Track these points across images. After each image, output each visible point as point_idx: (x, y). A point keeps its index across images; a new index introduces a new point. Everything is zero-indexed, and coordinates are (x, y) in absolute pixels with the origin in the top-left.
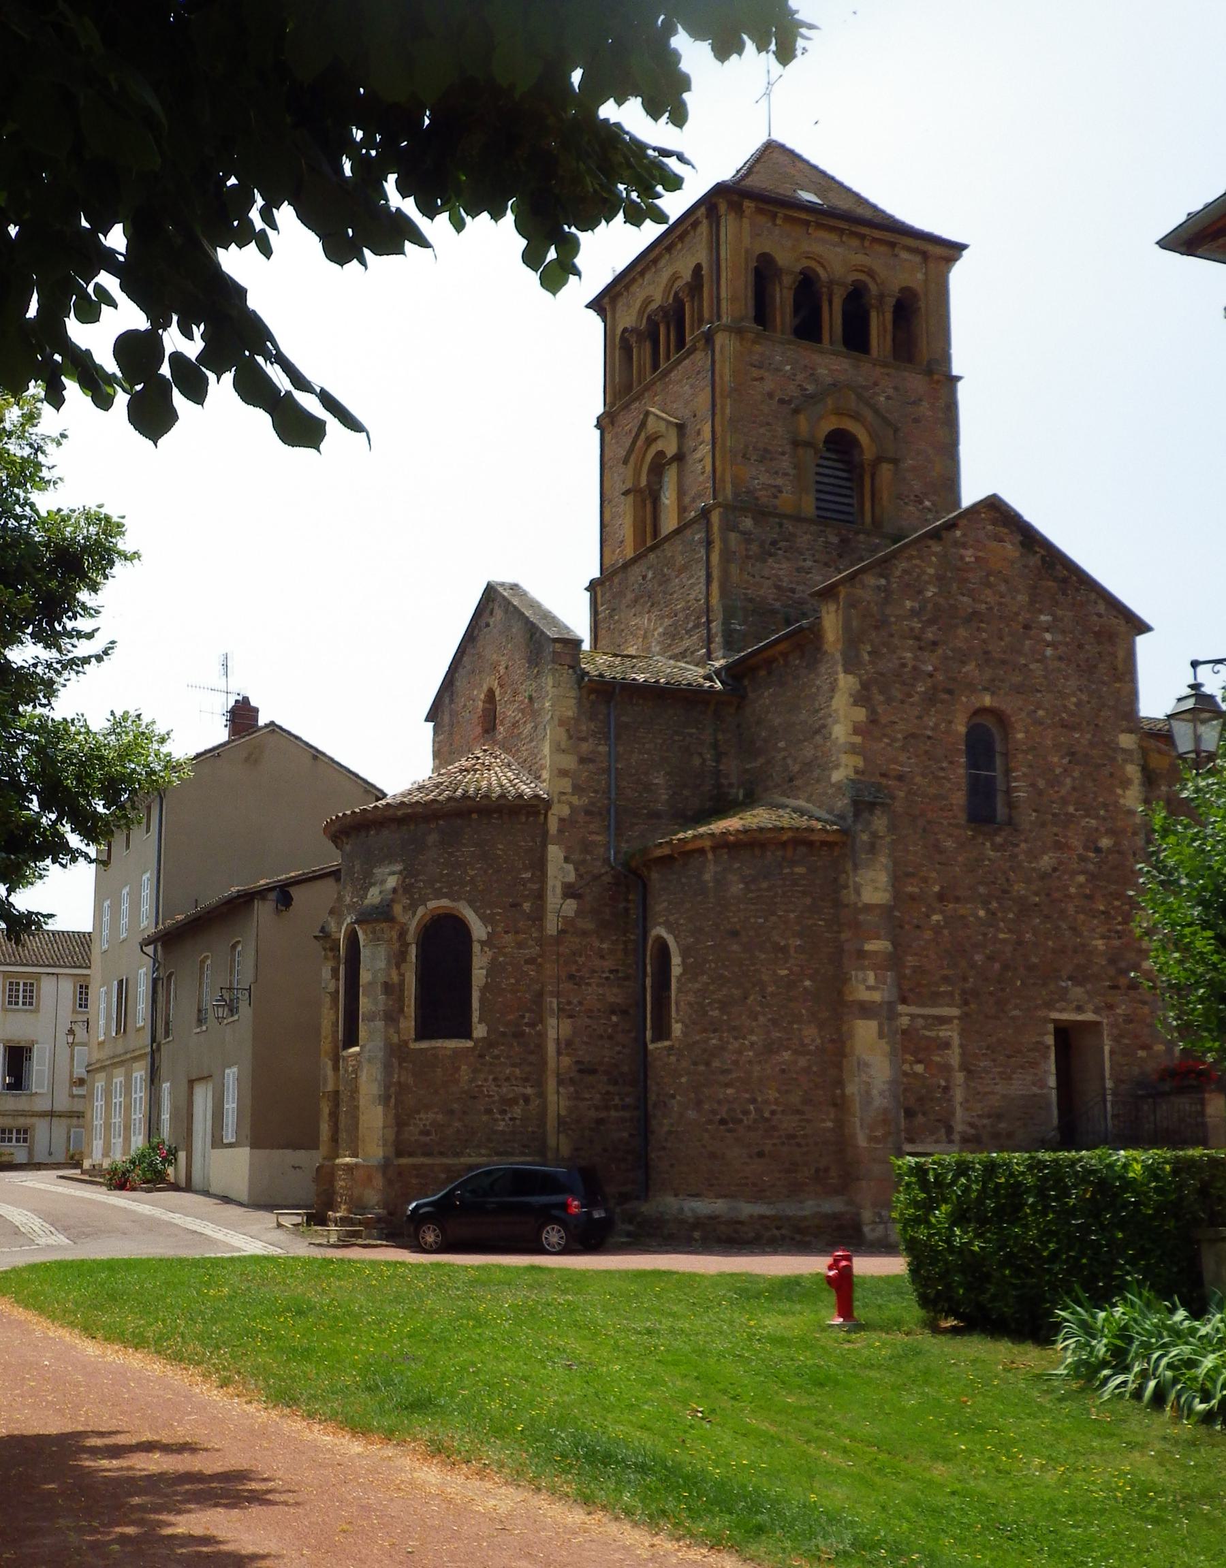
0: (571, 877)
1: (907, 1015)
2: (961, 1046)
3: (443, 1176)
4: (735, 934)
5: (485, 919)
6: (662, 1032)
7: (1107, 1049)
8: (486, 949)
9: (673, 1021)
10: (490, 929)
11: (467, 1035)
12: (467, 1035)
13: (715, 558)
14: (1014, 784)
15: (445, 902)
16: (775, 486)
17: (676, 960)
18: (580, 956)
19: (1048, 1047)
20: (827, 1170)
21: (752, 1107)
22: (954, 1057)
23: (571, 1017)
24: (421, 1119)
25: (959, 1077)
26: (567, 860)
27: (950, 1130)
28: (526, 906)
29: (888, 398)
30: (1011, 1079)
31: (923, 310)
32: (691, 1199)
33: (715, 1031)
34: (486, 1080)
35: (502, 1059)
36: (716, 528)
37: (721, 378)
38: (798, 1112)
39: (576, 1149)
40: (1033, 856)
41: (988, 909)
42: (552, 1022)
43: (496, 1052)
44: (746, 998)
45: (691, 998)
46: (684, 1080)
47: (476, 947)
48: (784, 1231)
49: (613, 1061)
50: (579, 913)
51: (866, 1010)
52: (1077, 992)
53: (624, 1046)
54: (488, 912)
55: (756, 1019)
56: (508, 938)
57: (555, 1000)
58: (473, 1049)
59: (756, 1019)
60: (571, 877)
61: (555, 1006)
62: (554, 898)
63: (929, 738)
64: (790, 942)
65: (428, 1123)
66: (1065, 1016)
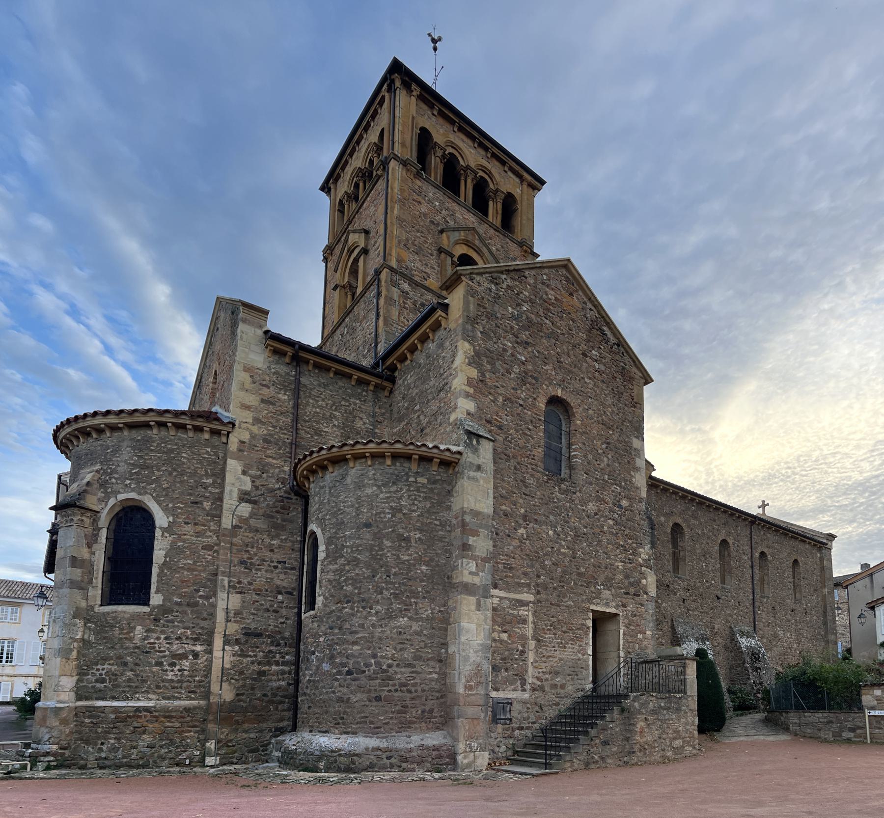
0: (248, 486)
1: (497, 597)
2: (534, 623)
3: (113, 716)
4: (368, 525)
5: (165, 510)
6: (312, 605)
7: (622, 631)
8: (166, 534)
9: (317, 595)
10: (171, 519)
11: (146, 603)
12: (146, 603)
13: (382, 301)
14: (573, 454)
15: (133, 495)
16: (425, 273)
17: (322, 548)
18: (253, 547)
19: (588, 628)
20: (431, 711)
21: (373, 661)
22: (529, 631)
23: (241, 593)
24: (98, 670)
25: (532, 644)
26: (244, 473)
27: (524, 682)
28: (207, 505)
29: (497, 250)
30: (565, 647)
31: (520, 209)
32: (321, 734)
33: (348, 602)
34: (158, 638)
35: (176, 623)
36: (383, 283)
37: (392, 189)
38: (409, 665)
39: (237, 695)
40: (584, 503)
41: (555, 531)
42: (222, 595)
43: (170, 617)
44: (374, 576)
45: (331, 576)
46: (321, 639)
47: (158, 533)
48: (393, 760)
49: (277, 629)
50: (252, 515)
51: (468, 589)
52: (607, 594)
53: (287, 619)
54: (170, 505)
55: (381, 593)
56: (188, 528)
57: (226, 579)
58: (150, 614)
59: (381, 593)
60: (248, 486)
61: (226, 583)
62: (230, 500)
63: (521, 405)
64: (412, 534)
65: (104, 672)
66: (599, 608)
